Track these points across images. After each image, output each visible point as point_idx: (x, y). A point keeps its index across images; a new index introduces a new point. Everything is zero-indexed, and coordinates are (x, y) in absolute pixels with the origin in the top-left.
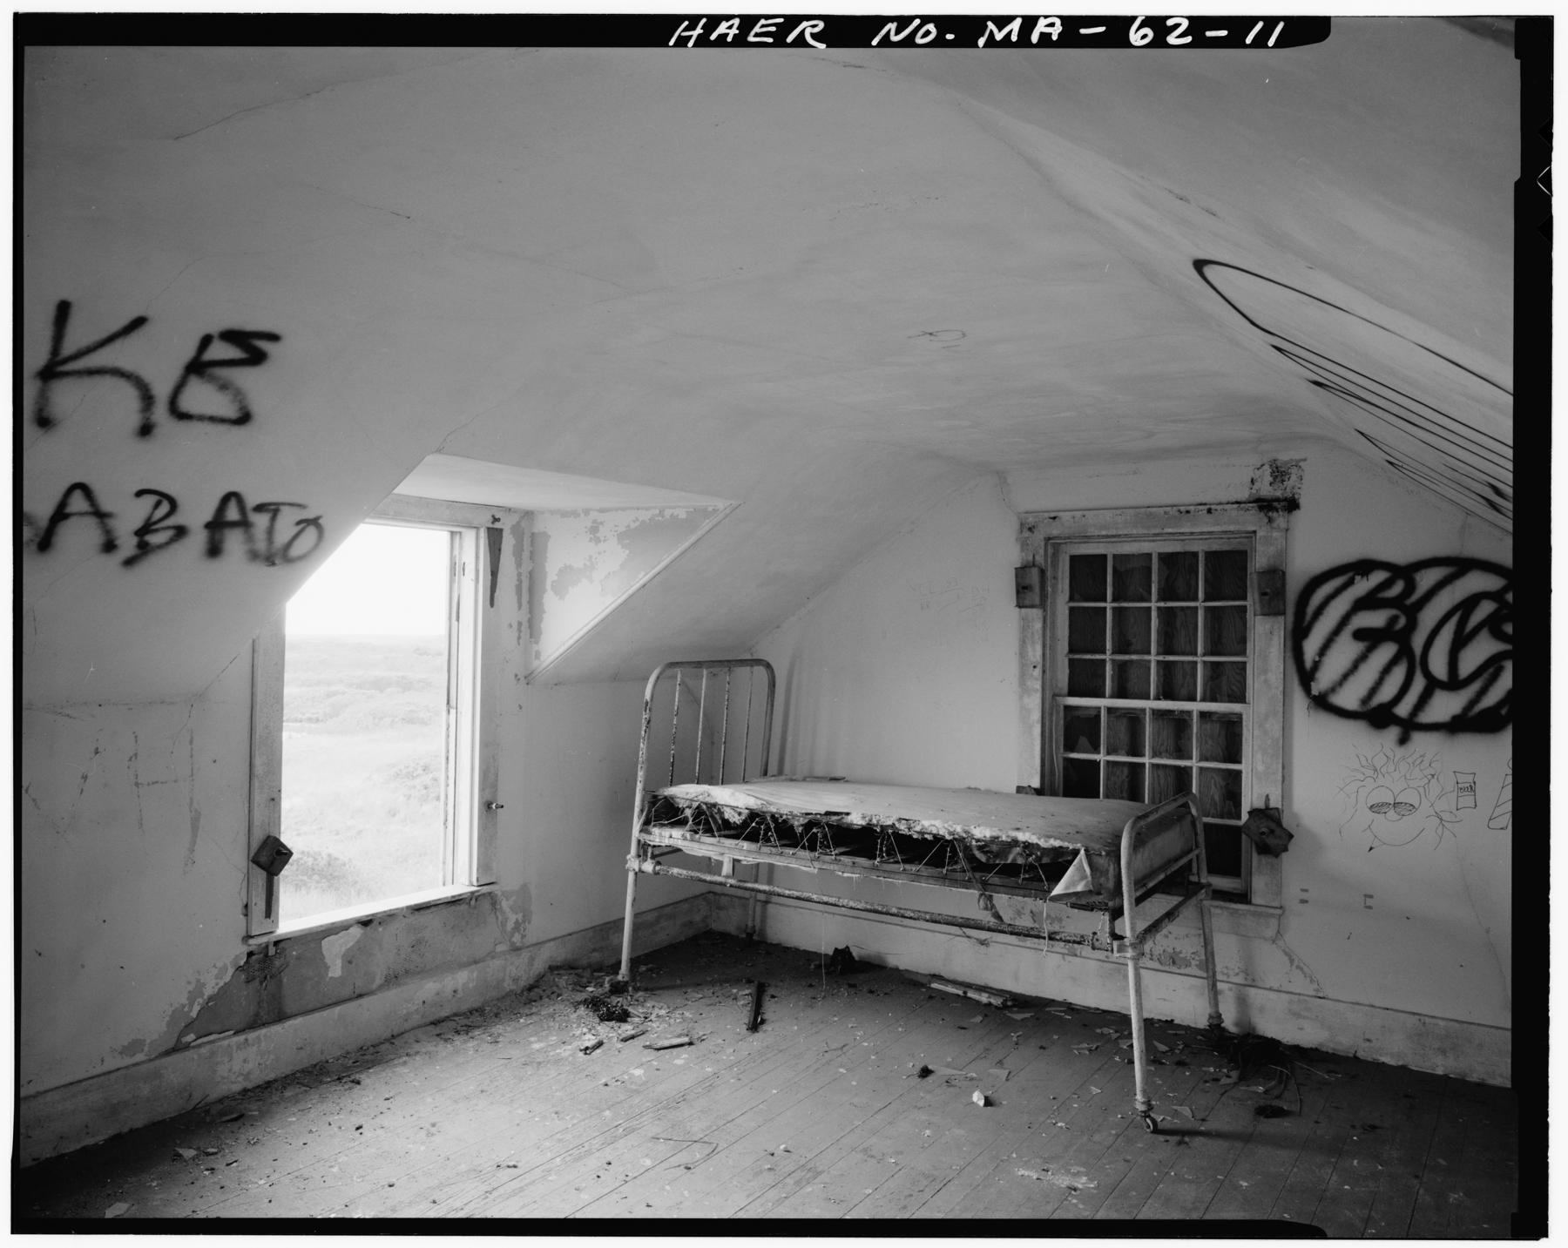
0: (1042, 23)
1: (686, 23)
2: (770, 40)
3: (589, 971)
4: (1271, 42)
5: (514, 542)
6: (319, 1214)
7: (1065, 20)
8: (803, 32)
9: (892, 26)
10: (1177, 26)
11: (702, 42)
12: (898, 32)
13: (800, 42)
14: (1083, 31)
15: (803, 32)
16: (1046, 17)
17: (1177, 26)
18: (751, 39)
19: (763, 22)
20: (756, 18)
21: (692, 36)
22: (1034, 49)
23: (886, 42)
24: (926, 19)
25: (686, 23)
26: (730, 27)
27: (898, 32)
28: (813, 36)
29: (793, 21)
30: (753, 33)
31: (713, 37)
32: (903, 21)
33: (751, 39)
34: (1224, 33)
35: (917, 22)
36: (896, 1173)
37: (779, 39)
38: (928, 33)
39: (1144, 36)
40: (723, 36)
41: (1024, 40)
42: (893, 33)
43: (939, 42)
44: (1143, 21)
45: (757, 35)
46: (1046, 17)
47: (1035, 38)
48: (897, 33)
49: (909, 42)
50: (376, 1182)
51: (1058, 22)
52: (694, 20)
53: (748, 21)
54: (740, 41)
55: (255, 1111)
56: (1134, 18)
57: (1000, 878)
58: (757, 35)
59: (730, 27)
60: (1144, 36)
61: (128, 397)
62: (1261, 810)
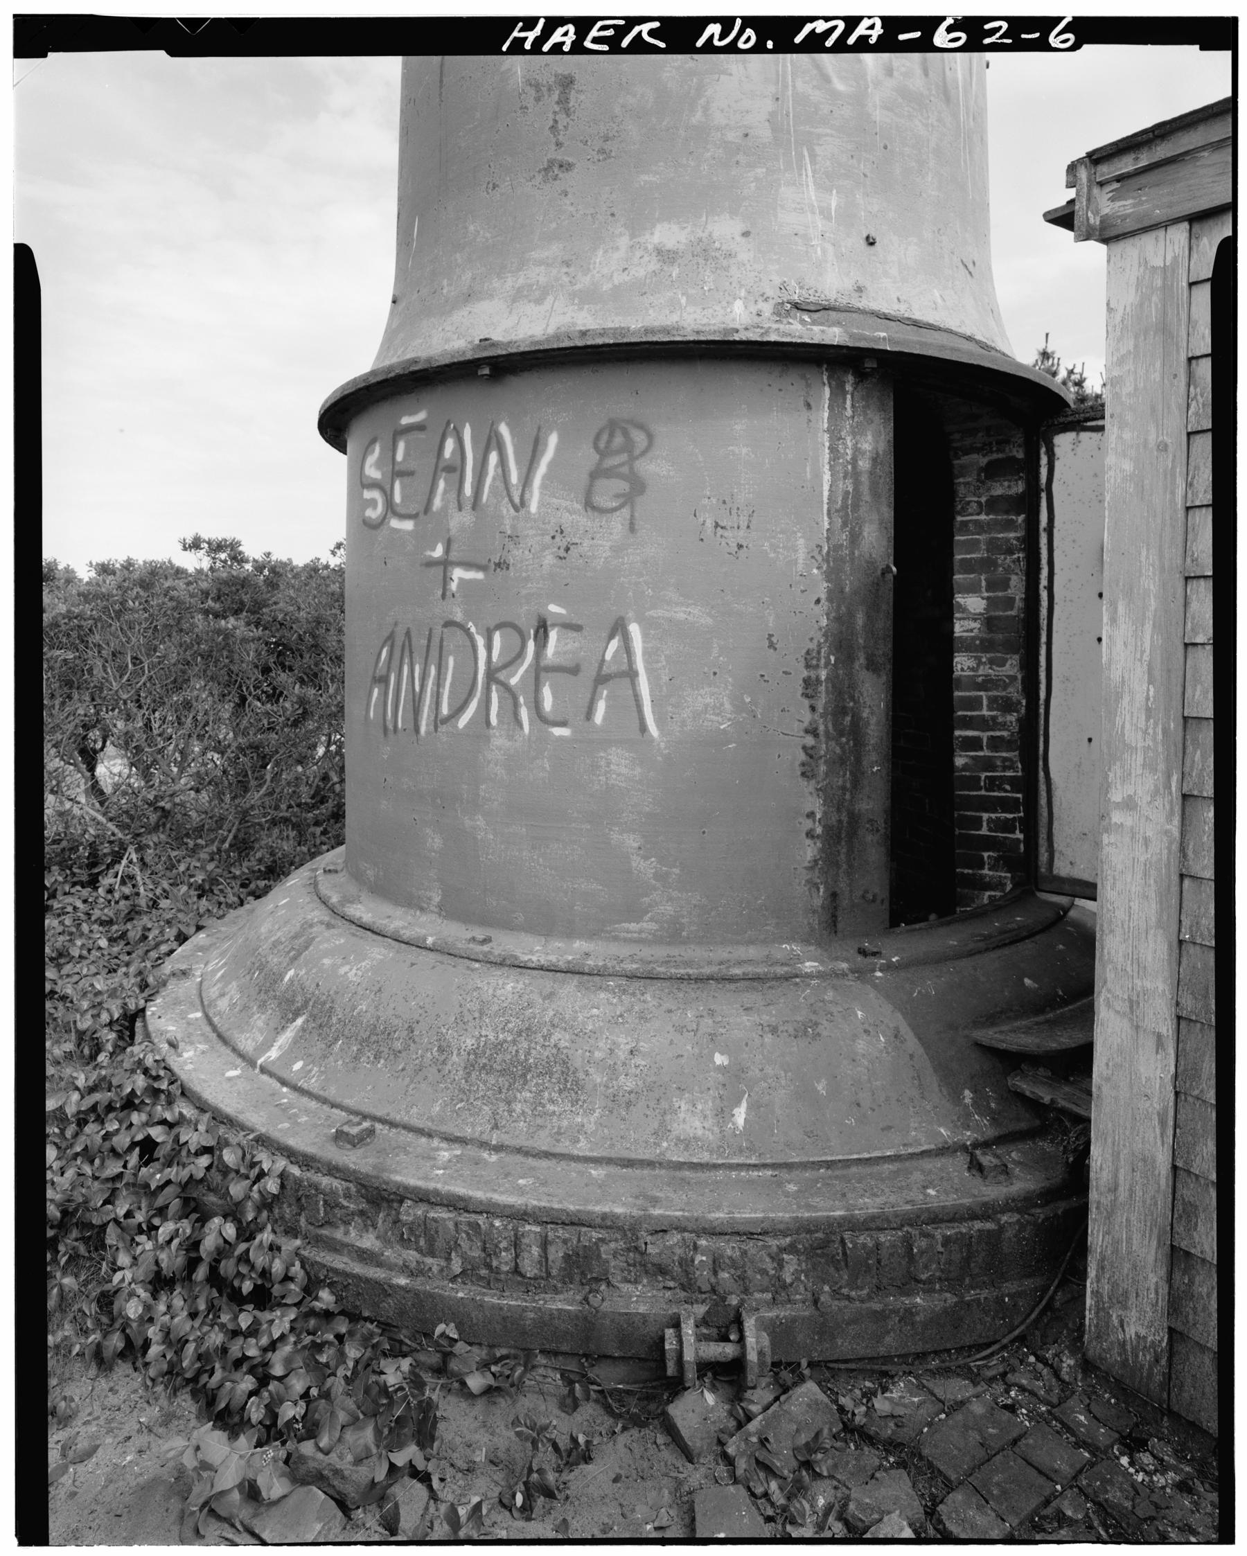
0: (866, 23)
1: (521, 24)
2: (605, 48)
3: (159, 814)
6: (529, 1537)
7: (886, 20)
9: (714, 29)
12: (721, 38)
13: (640, 46)
14: (1023, 36)
16: (870, 17)
19: (600, 24)
20: (594, 20)
21: (526, 38)
22: (505, 57)
23: (709, 48)
24: (748, 22)
25: (521, 24)
26: (566, 34)
27: (721, 38)
29: (633, 21)
30: (590, 37)
31: (851, 41)
32: (727, 23)
33: (588, 44)
36: (731, 1167)
37: (614, 45)
38: (748, 39)
39: (1066, 41)
40: (863, 39)
41: (537, 48)
42: (717, 37)
43: (759, 48)
44: (1069, 23)
45: (596, 40)
46: (870, 17)
48: (721, 39)
49: (732, 49)
51: (878, 23)
52: (530, 23)
53: (583, 24)
56: (1059, 20)
57: (823, 907)
58: (596, 40)
59: (872, 27)
60: (748, 39)
61: (1199, 1025)
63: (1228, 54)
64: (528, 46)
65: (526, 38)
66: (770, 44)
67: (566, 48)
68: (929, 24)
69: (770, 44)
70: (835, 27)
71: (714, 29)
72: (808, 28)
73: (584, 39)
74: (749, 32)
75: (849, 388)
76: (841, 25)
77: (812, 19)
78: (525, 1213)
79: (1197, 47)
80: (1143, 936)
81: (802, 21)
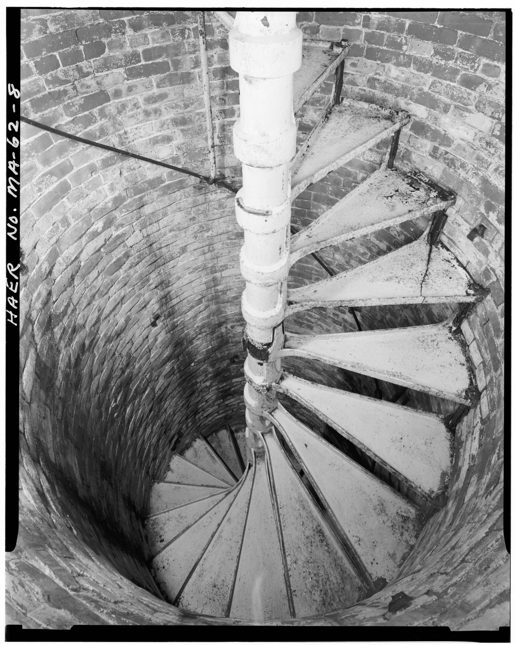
4: (18, 183)
5: (156, 484)
8: (13, 272)
9: (10, 234)
10: (12, 127)
11: (18, 178)
15: (13, 272)
17: (12, 127)
18: (15, 291)
24: (8, 221)
28: (14, 267)
29: (8, 275)
31: (16, 308)
32: (9, 230)
33: (15, 291)
34: (14, 106)
35: (9, 225)
38: (14, 220)
40: (16, 304)
43: (17, 215)
45: (14, 288)
47: (16, 308)
49: (18, 226)
50: (211, 601)
52: (8, 316)
53: (9, 293)
54: (17, 296)
55: (486, 439)
56: (7, 143)
58: (14, 288)
59: (11, 301)
60: (14, 220)
62: (294, 374)
63: (22, 10)
64: (16, 316)
65: (13, 235)
66: (15, 210)
67: (18, 166)
68: (10, 149)
69: (15, 210)
70: (12, 181)
71: (10, 234)
72: (10, 192)
73: (13, 292)
74: (11, 218)
75: (125, 482)
76: (10, 178)
77: (7, 190)
78: (436, 185)
79: (24, 627)
80: (309, 323)
81: (8, 195)
